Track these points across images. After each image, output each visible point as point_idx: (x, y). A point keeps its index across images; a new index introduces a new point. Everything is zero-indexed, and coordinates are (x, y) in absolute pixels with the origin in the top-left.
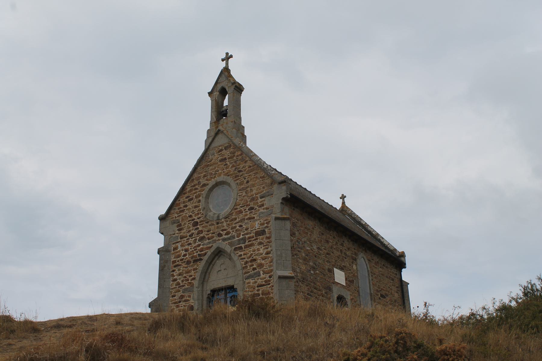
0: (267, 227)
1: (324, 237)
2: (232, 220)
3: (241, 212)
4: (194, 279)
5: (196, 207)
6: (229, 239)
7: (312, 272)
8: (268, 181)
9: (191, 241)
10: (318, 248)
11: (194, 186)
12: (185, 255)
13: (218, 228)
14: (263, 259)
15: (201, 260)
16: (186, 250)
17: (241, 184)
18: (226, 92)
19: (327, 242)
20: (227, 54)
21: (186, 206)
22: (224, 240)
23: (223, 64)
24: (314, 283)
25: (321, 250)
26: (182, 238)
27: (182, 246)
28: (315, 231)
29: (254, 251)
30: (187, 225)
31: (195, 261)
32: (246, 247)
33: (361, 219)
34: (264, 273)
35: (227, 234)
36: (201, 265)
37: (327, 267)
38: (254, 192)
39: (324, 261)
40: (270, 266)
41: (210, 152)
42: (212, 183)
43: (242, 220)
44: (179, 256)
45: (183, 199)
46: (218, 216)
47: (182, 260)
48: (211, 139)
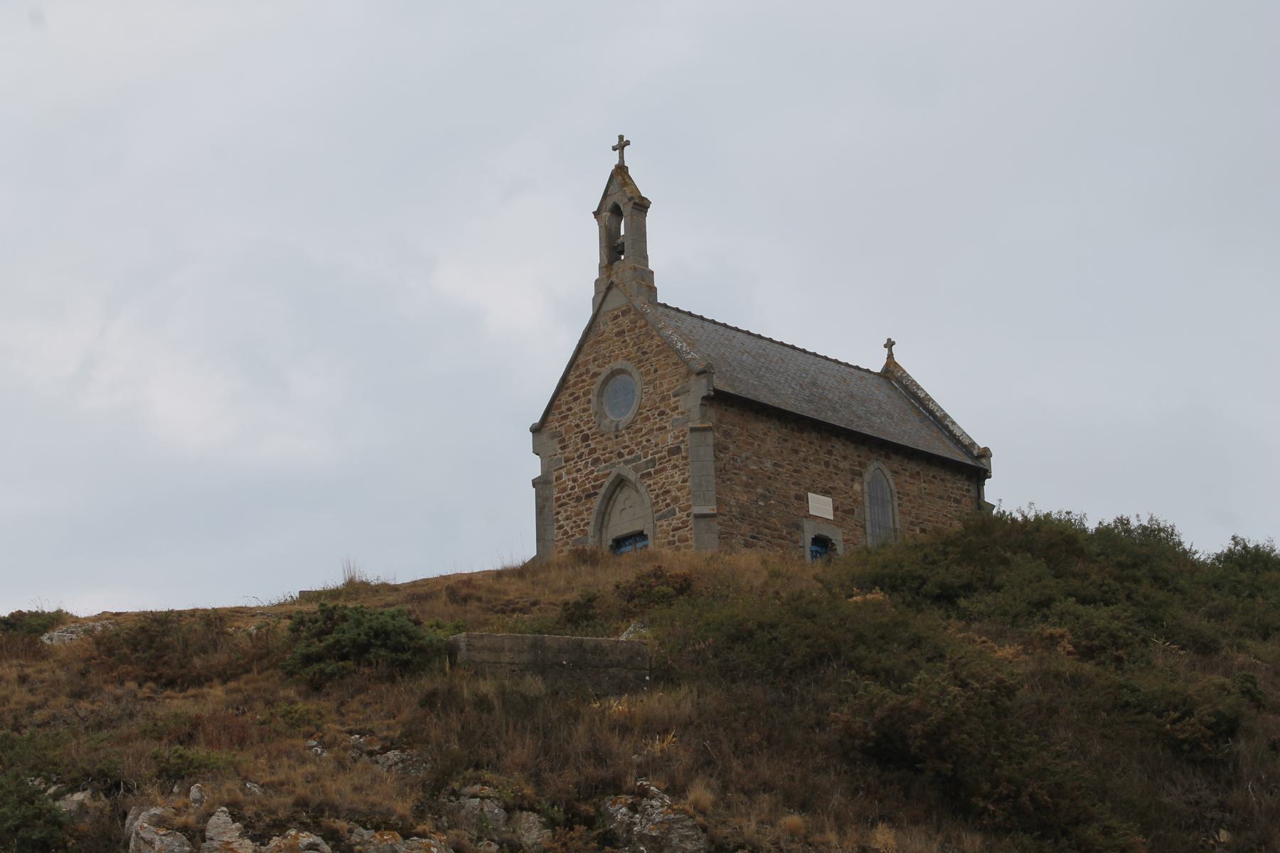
0: (683, 442)
1: (789, 445)
2: (636, 432)
3: (647, 419)
4: (588, 524)
5: (585, 410)
6: (633, 461)
7: (761, 503)
8: (683, 370)
9: (581, 465)
10: (775, 465)
11: (581, 375)
12: (573, 488)
13: (617, 443)
14: (680, 489)
15: (596, 494)
16: (575, 480)
17: (647, 373)
18: (622, 210)
19: (796, 452)
20: (621, 137)
21: (570, 409)
22: (626, 462)
23: (614, 159)
24: (765, 520)
25: (782, 467)
26: (567, 460)
27: (568, 473)
28: (770, 437)
29: (667, 478)
30: (574, 440)
31: (588, 497)
32: (656, 472)
33: (918, 387)
34: (681, 510)
35: (631, 453)
36: (596, 503)
37: (793, 493)
38: (666, 386)
39: (787, 483)
40: (688, 500)
41: (601, 319)
42: (605, 371)
43: (650, 431)
44: (564, 490)
45: (565, 397)
46: (617, 426)
47: (569, 495)
48: (601, 296)
